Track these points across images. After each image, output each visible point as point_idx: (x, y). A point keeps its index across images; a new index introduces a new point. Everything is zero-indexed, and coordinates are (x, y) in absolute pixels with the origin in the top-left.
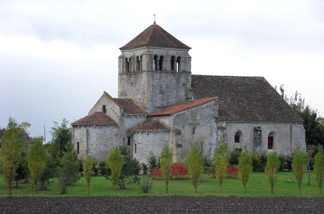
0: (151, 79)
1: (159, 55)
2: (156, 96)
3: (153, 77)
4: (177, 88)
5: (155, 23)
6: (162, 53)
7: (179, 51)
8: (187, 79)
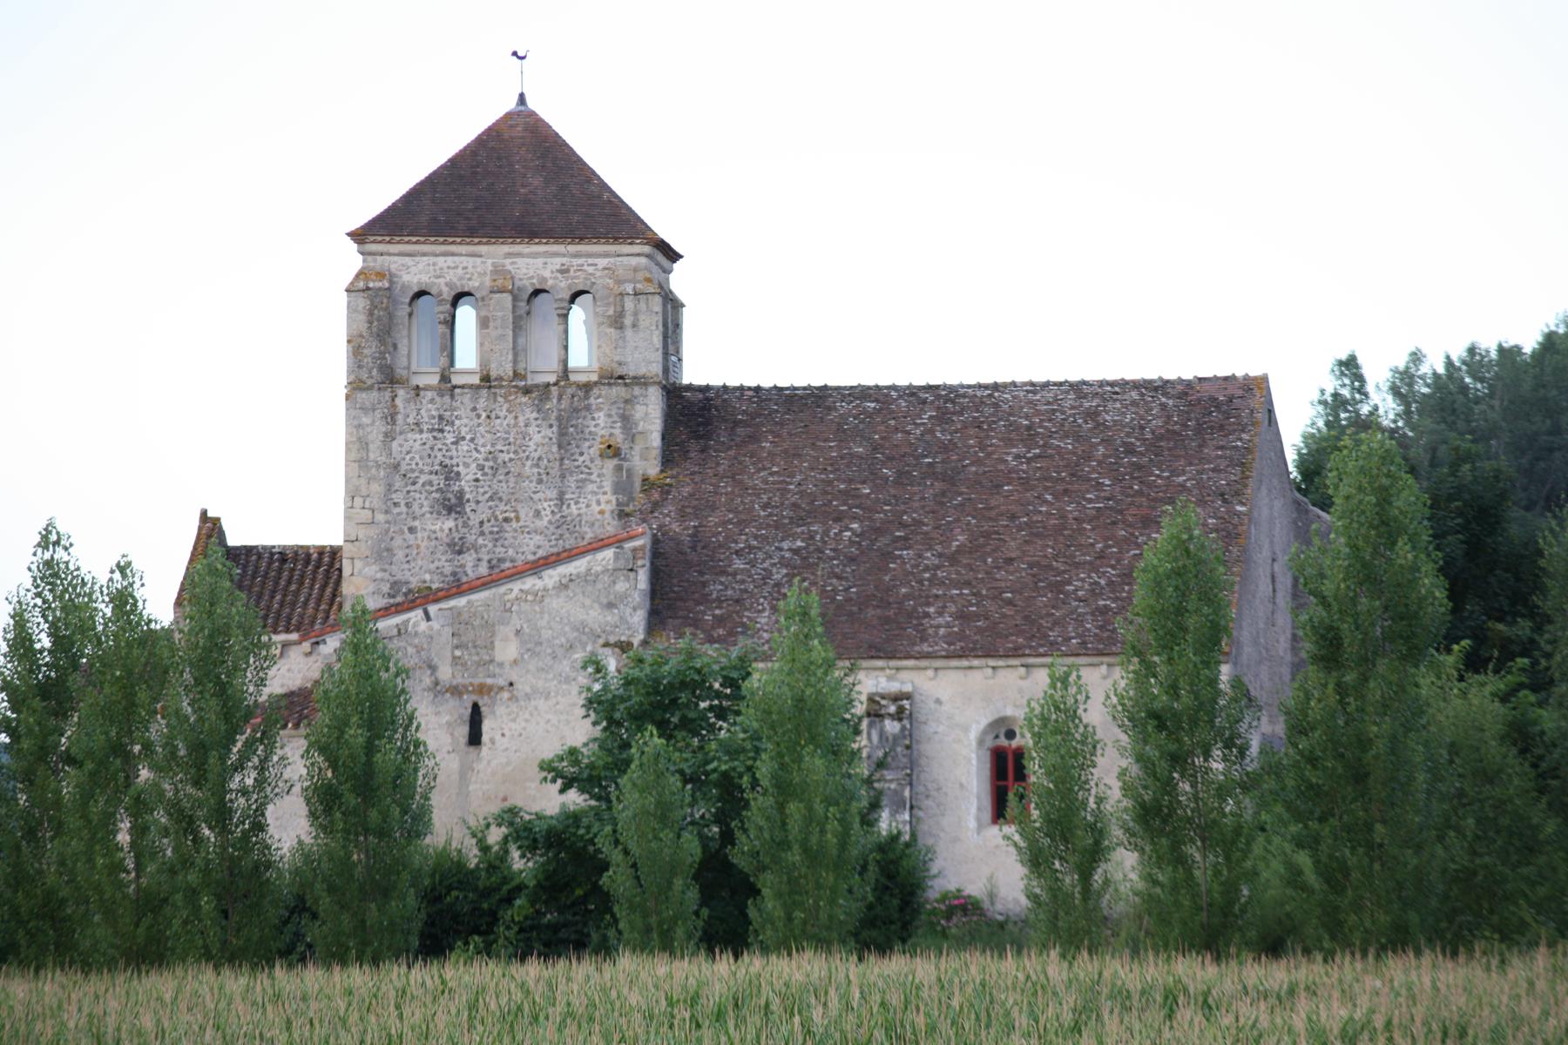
0: (376, 431)
1: (445, 289)
2: (412, 530)
3: (391, 417)
4: (563, 477)
5: (522, 99)
6: (461, 279)
7: (576, 261)
8: (626, 419)
